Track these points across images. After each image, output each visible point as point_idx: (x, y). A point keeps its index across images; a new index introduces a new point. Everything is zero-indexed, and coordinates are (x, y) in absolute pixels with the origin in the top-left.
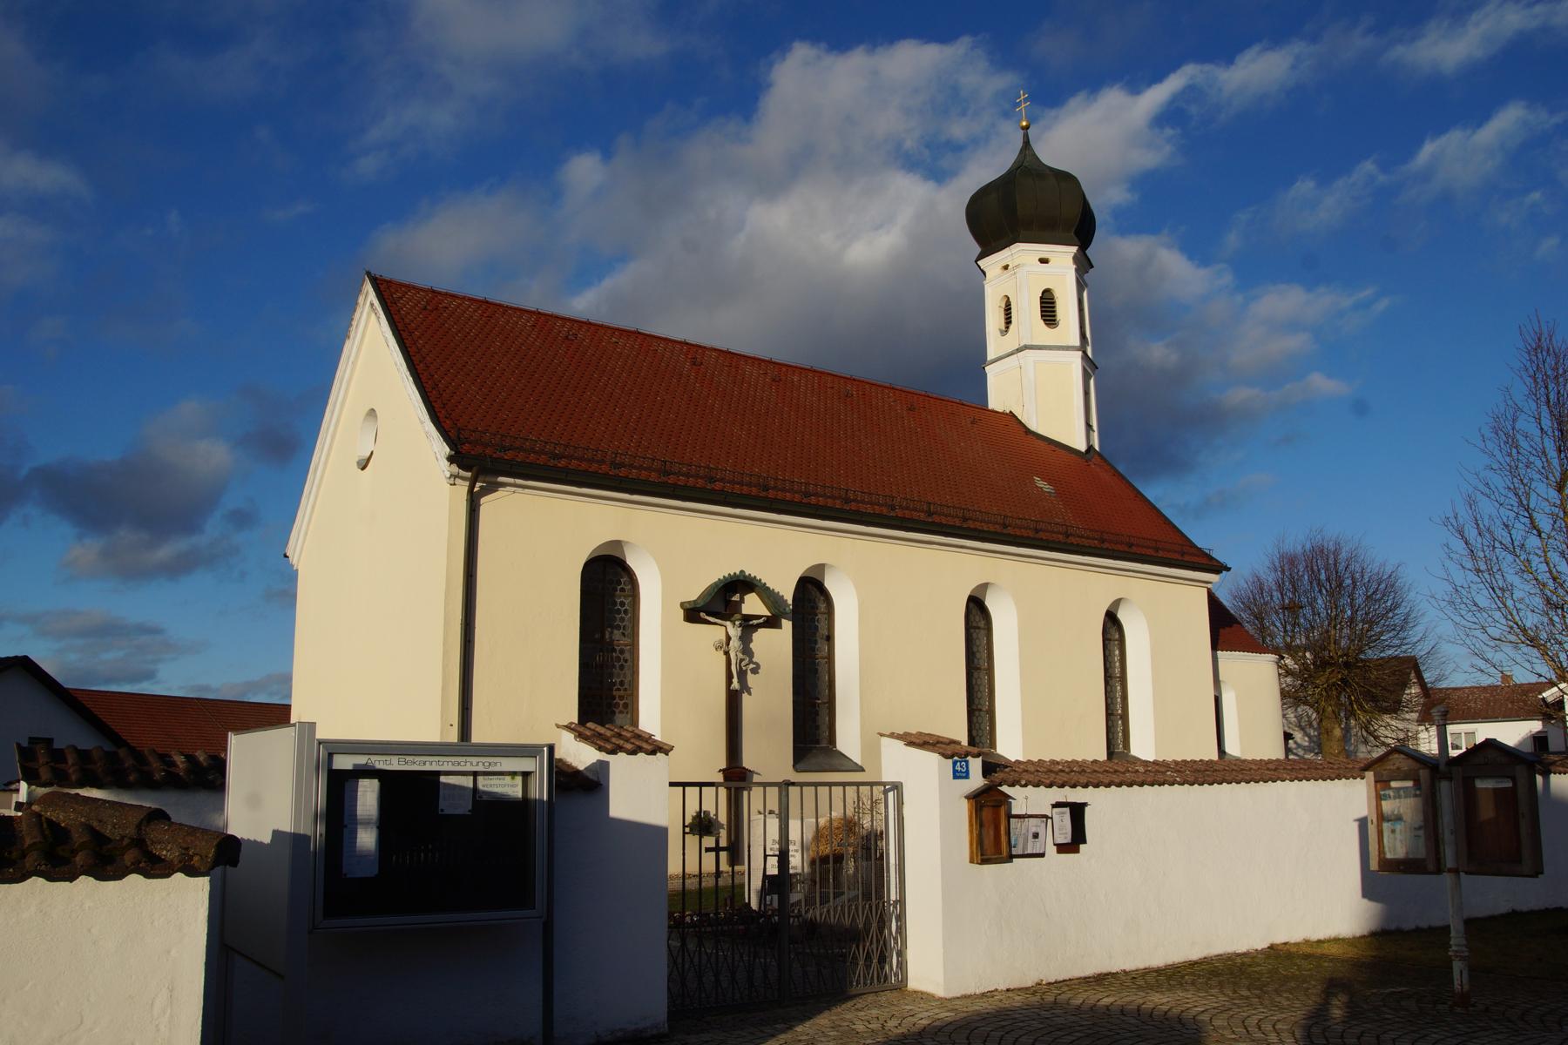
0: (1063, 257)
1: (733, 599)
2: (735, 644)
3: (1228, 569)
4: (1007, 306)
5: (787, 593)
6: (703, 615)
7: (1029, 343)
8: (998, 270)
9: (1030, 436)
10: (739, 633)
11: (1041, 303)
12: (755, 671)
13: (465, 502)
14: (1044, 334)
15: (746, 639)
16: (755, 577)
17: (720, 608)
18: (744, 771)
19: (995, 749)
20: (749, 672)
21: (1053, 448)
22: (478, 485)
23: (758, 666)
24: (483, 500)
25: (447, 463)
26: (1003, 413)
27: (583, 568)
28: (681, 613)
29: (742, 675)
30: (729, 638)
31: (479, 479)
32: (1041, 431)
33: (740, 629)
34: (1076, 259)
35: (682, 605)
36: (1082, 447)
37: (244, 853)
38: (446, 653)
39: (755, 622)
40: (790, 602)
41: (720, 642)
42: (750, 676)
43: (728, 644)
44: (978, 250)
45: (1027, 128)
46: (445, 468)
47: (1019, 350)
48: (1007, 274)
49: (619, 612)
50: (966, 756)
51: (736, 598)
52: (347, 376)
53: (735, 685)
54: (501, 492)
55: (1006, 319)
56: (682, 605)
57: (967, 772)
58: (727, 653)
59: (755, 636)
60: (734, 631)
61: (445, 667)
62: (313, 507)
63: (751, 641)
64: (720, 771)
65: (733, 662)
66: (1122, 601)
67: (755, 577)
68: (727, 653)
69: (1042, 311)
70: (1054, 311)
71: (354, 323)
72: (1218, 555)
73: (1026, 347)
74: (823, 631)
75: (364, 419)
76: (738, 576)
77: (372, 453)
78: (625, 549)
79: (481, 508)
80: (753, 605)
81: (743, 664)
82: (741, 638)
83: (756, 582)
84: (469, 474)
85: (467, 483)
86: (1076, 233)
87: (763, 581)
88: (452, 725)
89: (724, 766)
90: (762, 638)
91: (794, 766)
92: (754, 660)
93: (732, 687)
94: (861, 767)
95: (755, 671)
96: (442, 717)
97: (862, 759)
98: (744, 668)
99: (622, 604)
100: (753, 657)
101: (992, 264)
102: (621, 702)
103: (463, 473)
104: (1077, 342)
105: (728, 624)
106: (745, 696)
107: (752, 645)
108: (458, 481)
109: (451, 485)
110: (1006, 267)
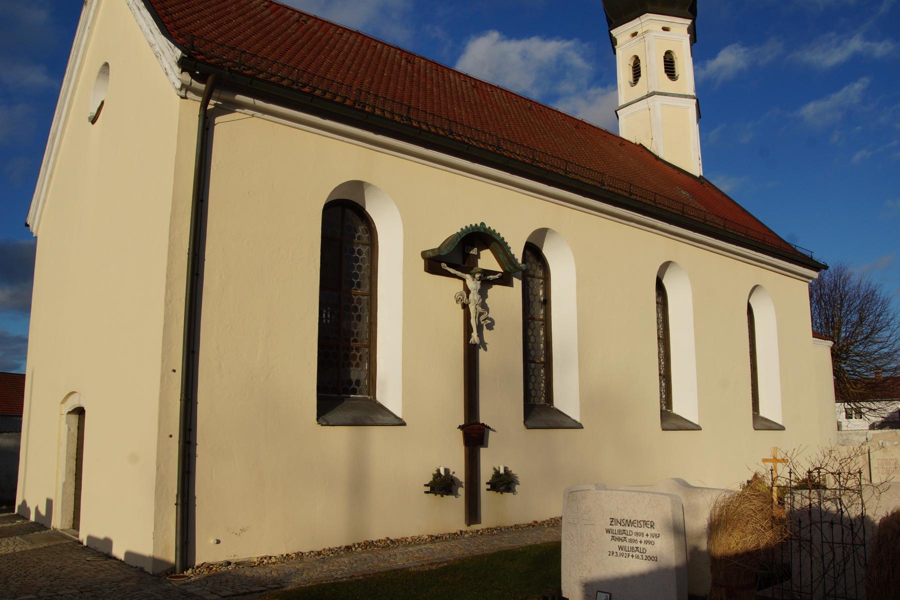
0: (680, 27)
1: (471, 252)
2: (474, 297)
3: (826, 267)
5: (517, 252)
6: (444, 265)
8: (628, 36)
9: (659, 162)
10: (479, 287)
11: (665, 61)
12: (490, 327)
13: (197, 118)
17: (458, 260)
19: (671, 408)
22: (212, 102)
24: (218, 120)
25: (177, 70)
26: (635, 144)
27: (323, 212)
28: (421, 263)
33: (479, 282)
35: (423, 254)
37: (528, 241)
39: (492, 277)
42: (486, 331)
46: (176, 77)
51: (474, 252)
52: (83, 42)
54: (238, 115)
56: (423, 254)
58: (465, 307)
60: (473, 284)
61: (168, 302)
62: (51, 176)
65: (473, 315)
70: (674, 69)
75: (98, 77)
76: (479, 228)
77: (103, 103)
78: (366, 193)
79: (216, 127)
80: (487, 260)
83: (494, 236)
84: (202, 87)
85: (200, 99)
86: (690, 10)
87: (502, 236)
88: (174, 371)
89: (462, 423)
90: (496, 292)
91: (524, 422)
93: (472, 341)
94: (580, 424)
95: (490, 327)
96: (163, 361)
97: (405, 408)
98: (482, 323)
99: (360, 252)
101: (621, 33)
103: (196, 84)
105: (468, 277)
108: (190, 95)
109: (182, 97)
110: (634, 34)
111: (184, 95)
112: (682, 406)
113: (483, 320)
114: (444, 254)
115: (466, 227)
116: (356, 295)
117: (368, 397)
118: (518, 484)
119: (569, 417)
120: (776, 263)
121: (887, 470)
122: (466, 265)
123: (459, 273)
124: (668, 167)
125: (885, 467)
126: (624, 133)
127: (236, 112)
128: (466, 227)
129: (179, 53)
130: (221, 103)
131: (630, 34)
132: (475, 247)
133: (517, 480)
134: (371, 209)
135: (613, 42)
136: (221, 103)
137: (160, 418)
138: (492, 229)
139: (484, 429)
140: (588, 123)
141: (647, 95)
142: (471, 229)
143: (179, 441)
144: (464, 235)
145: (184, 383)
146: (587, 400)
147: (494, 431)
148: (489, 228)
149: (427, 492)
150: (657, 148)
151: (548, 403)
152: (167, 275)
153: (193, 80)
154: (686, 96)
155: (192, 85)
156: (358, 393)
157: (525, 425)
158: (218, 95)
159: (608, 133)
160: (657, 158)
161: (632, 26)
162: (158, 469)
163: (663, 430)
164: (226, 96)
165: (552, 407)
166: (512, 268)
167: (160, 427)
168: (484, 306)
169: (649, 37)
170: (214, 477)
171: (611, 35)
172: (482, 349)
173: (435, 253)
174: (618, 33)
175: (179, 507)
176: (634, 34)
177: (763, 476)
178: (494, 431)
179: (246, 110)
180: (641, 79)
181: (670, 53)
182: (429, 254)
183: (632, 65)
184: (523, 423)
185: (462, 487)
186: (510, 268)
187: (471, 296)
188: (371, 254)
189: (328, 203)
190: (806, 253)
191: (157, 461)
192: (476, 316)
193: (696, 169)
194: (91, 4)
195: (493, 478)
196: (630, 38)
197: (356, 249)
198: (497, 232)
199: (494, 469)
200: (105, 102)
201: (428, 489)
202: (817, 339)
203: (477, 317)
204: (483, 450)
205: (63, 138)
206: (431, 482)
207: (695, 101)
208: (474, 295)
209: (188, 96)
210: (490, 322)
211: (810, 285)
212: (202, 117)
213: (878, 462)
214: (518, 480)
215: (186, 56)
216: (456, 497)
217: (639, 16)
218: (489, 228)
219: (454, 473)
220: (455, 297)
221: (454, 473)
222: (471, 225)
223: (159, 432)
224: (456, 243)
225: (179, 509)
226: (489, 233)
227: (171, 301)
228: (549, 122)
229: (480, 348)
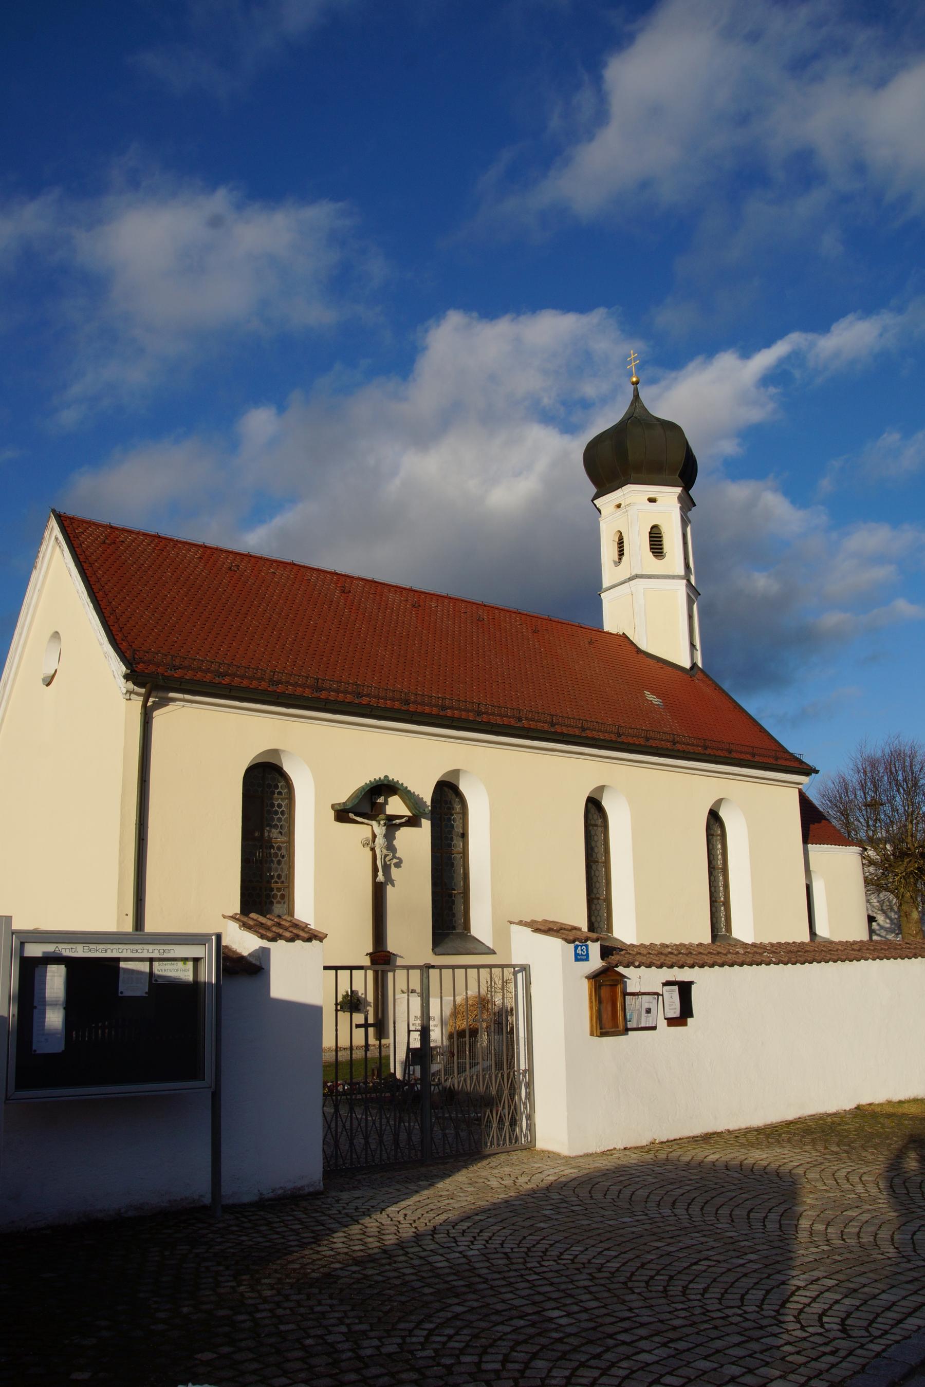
0: (670, 496)
1: (378, 801)
2: (380, 841)
3: (817, 772)
4: (620, 540)
5: (426, 794)
6: (351, 815)
7: (639, 572)
10: (384, 832)
11: (650, 537)
12: (398, 865)
14: (651, 564)
15: (389, 836)
16: (398, 781)
17: (367, 809)
19: (612, 933)
20: (392, 866)
21: (661, 665)
22: (151, 700)
23: (401, 861)
24: (155, 713)
25: (124, 681)
28: (332, 813)
29: (386, 868)
30: (374, 836)
31: (152, 695)
33: (384, 828)
34: (680, 498)
35: (333, 806)
36: (687, 665)
38: (122, 850)
39: (398, 821)
41: (367, 839)
43: (374, 842)
44: (593, 490)
45: (637, 383)
46: (122, 685)
48: (620, 511)
50: (586, 940)
51: (381, 800)
53: (381, 877)
54: (172, 707)
56: (333, 806)
57: (587, 955)
58: (373, 849)
64: (367, 954)
67: (398, 781)
68: (373, 849)
73: (637, 576)
75: (50, 641)
80: (396, 806)
81: (387, 859)
82: (385, 836)
83: (397, 786)
84: (143, 691)
85: (142, 698)
86: (681, 476)
88: (127, 915)
89: (371, 950)
90: (404, 835)
92: (397, 855)
95: (398, 865)
96: (118, 908)
98: (388, 863)
99: (280, 806)
101: (606, 502)
102: (279, 894)
103: (137, 689)
104: (681, 571)
105: (374, 823)
106: (389, 887)
108: (133, 696)
109: (127, 700)
110: (619, 506)
116: (276, 843)
119: (483, 944)
129: (124, 669)
131: (614, 506)
132: (381, 796)
134: (287, 768)
138: (395, 780)
139: (390, 957)
144: (368, 788)
147: (402, 957)
151: (465, 930)
153: (135, 687)
160: (639, 651)
164: (161, 694)
168: (391, 847)
172: (390, 885)
178: (402, 957)
180: (624, 558)
184: (431, 951)
185: (371, 1006)
187: (377, 840)
188: (290, 806)
189: (251, 766)
194: (41, 569)
197: (276, 803)
200: (58, 670)
202: (833, 846)
208: (379, 839)
210: (398, 861)
217: (621, 487)
222: (375, 779)
224: (361, 797)
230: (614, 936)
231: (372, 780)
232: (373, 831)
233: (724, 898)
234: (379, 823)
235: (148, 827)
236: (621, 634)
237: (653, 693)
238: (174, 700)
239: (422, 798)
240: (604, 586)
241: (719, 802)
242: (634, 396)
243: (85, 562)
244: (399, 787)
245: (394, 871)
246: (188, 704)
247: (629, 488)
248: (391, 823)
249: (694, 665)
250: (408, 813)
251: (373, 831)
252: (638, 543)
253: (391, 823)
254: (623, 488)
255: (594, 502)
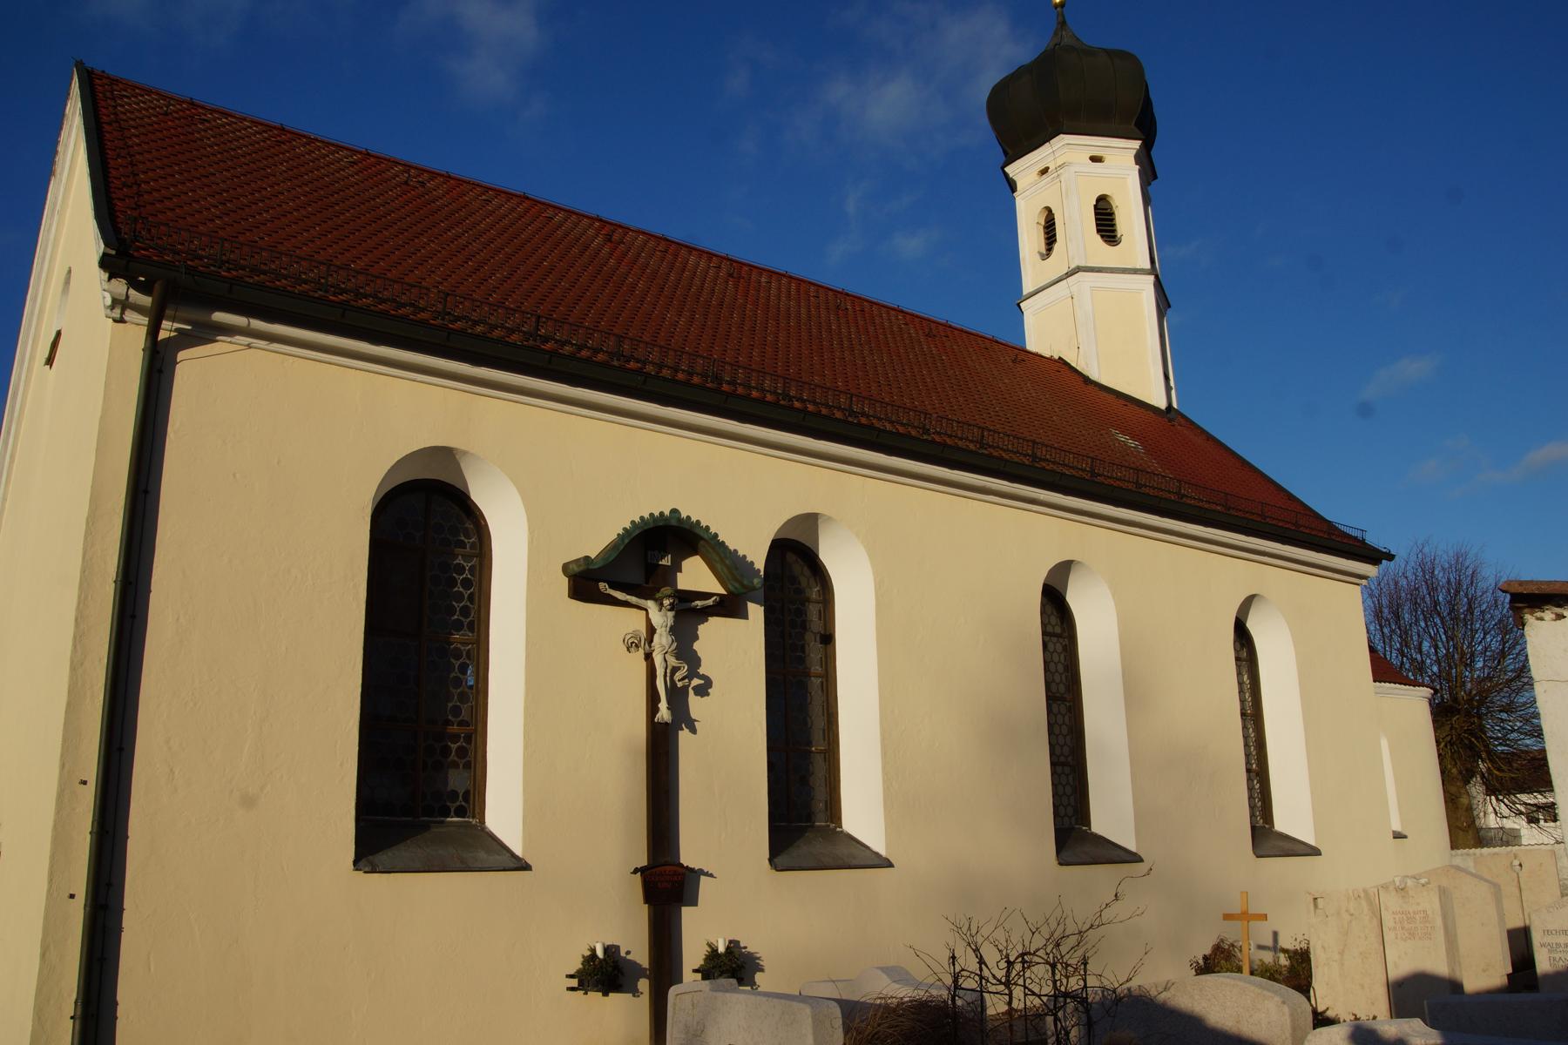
0: (1121, 155)
2: (662, 640)
4: (1047, 222)
5: (757, 555)
6: (603, 586)
7: (1083, 264)
9: (1090, 387)
10: (670, 622)
11: (1096, 214)
12: (702, 691)
14: (1102, 253)
15: (684, 635)
16: (698, 522)
17: (636, 576)
18: (680, 870)
19: (1088, 824)
20: (691, 692)
22: (166, 324)
23: (708, 683)
24: (181, 355)
26: (1051, 359)
28: (563, 583)
29: (678, 697)
30: (651, 630)
31: (168, 312)
32: (1104, 382)
33: (671, 614)
34: (1138, 159)
38: (79, 638)
39: (699, 603)
40: (760, 564)
41: (635, 635)
43: (650, 640)
44: (1003, 158)
47: (1069, 274)
48: (1046, 178)
49: (460, 597)
51: (666, 561)
52: (52, 237)
53: (664, 713)
54: (222, 345)
55: (1047, 239)
58: (649, 657)
59: (703, 629)
60: (661, 618)
63: (696, 638)
64: (636, 871)
66: (1256, 599)
67: (698, 522)
68: (649, 657)
69: (1097, 225)
70: (1114, 225)
71: (60, 149)
72: (1374, 539)
73: (1078, 270)
74: (816, 625)
76: (667, 519)
77: (59, 334)
78: (462, 465)
80: (696, 575)
81: (678, 676)
82: (673, 630)
83: (697, 531)
84: (146, 300)
85: (145, 320)
86: (1138, 125)
88: (85, 783)
89: (643, 861)
91: (770, 860)
92: (701, 671)
96: (63, 766)
98: (679, 684)
100: (699, 665)
101: (1023, 170)
102: (454, 746)
104: (1148, 266)
105: (650, 605)
106: (684, 735)
107: (696, 646)
108: (130, 315)
109: (115, 321)
110: (1044, 171)
111: (119, 316)
112: (1290, 818)
113: (679, 681)
114: (596, 567)
115: (642, 518)
117: (471, 820)
118: (762, 970)
120: (1339, 567)
121: (1410, 934)
122: (650, 585)
123: (633, 599)
124: (1105, 394)
125: (1407, 926)
126: (1032, 345)
127: (217, 341)
128: (642, 518)
130: (189, 328)
133: (758, 963)
135: (1012, 186)
136: (189, 328)
137: (52, 866)
138: (694, 519)
139: (684, 874)
140: (959, 327)
141: (1067, 274)
142: (651, 521)
143: (85, 905)
144: (637, 532)
145: (98, 802)
146: (1143, 818)
147: (711, 875)
148: (689, 517)
149: (572, 989)
150: (1087, 365)
151: (832, 822)
152: (76, 620)
153: (132, 292)
154: (1135, 271)
155: (130, 299)
156: (452, 814)
157: (771, 865)
158: (173, 313)
159: (997, 342)
160: (1087, 380)
161: (1040, 158)
162: (43, 955)
163: (1061, 864)
165: (838, 829)
166: (737, 585)
167: (51, 880)
169: (1065, 174)
170: (152, 969)
171: (1006, 175)
173: (580, 565)
174: (1017, 171)
175: (78, 1022)
176: (1044, 171)
177: (1233, 945)
178: (711, 875)
179: (237, 337)
180: (1056, 247)
181: (1105, 199)
182: (573, 569)
183: (1043, 223)
186: (736, 588)
187: (656, 638)
190: (1354, 533)
191: (44, 940)
192: (666, 673)
193: (1156, 397)
194: (61, 174)
195: (705, 960)
196: (1037, 178)
198: (704, 524)
199: (709, 945)
201: (574, 983)
203: (668, 675)
204: (687, 912)
205: (26, 398)
206: (578, 971)
207: (1151, 278)
209: (126, 318)
210: (702, 682)
211: (1369, 593)
212: (147, 353)
213: (1395, 918)
214: (761, 963)
215: (113, 252)
216: (634, 996)
217: (1048, 141)
218: (689, 517)
219: (628, 953)
220: (624, 641)
221: (628, 953)
223: (49, 891)
224: (622, 547)
225: (77, 1027)
226: (687, 527)
227: (82, 664)
228: (871, 329)
229: (682, 729)
230: (1093, 830)
231: (646, 516)
232: (648, 621)
233: (1257, 766)
234: (661, 605)
235: (149, 591)
236: (1057, 358)
237: (1122, 433)
238: (229, 330)
239: (745, 556)
240: (1025, 292)
241: (1063, 570)
242: (1059, 23)
243: (122, 135)
244: (702, 533)
245: (696, 704)
246: (262, 344)
247: (1062, 140)
248: (685, 606)
249: (1170, 407)
250: (718, 589)
251: (648, 621)
252: (1078, 225)
253: (685, 606)
254: (1052, 141)
255: (1007, 169)
